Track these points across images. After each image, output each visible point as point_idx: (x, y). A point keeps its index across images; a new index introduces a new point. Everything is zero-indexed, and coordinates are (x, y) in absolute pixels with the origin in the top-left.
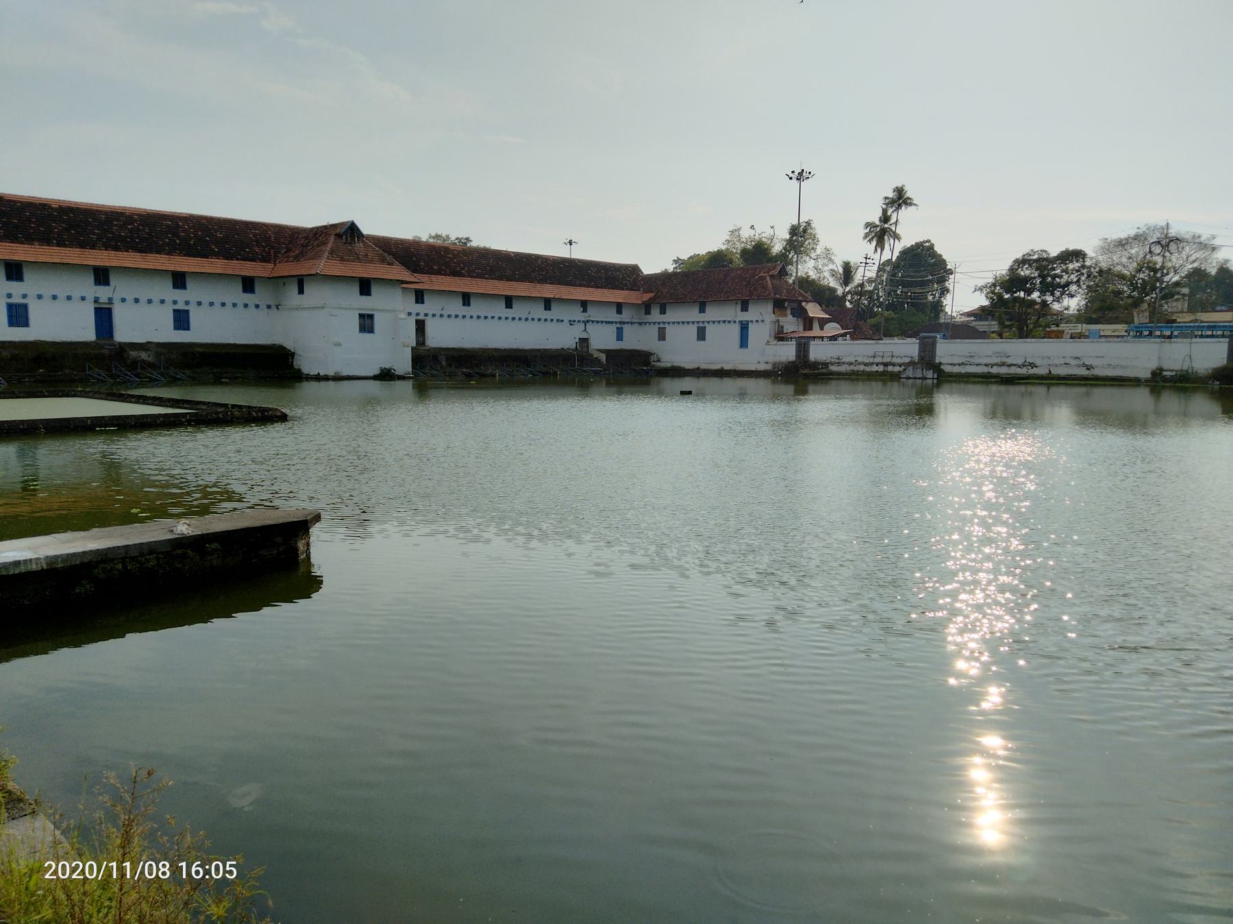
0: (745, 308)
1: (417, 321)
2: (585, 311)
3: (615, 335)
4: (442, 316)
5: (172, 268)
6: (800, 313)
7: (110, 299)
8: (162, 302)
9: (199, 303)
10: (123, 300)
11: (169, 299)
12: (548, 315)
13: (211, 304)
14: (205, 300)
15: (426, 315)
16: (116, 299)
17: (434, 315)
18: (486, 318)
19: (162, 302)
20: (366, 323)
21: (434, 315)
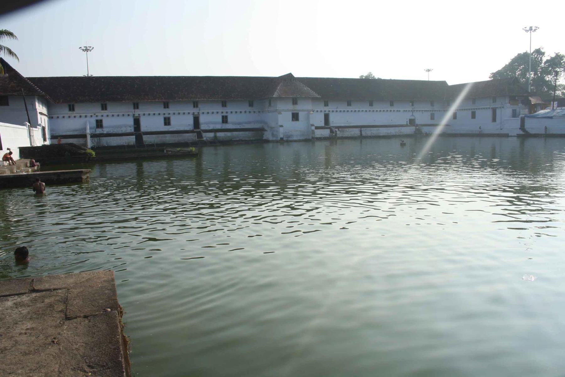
0: (494, 101)
1: (223, 117)
2: (413, 105)
3: (430, 117)
4: (337, 111)
5: (491, 107)
6: (527, 103)
7: (198, 113)
8: (159, 114)
9: (174, 114)
10: (203, 113)
11: (220, 111)
12: (350, 108)
13: (241, 112)
14: (234, 111)
15: (227, 112)
16: (201, 112)
17: (333, 111)
18: (344, 111)
19: (218, 113)
20: (295, 117)
21: (333, 111)
